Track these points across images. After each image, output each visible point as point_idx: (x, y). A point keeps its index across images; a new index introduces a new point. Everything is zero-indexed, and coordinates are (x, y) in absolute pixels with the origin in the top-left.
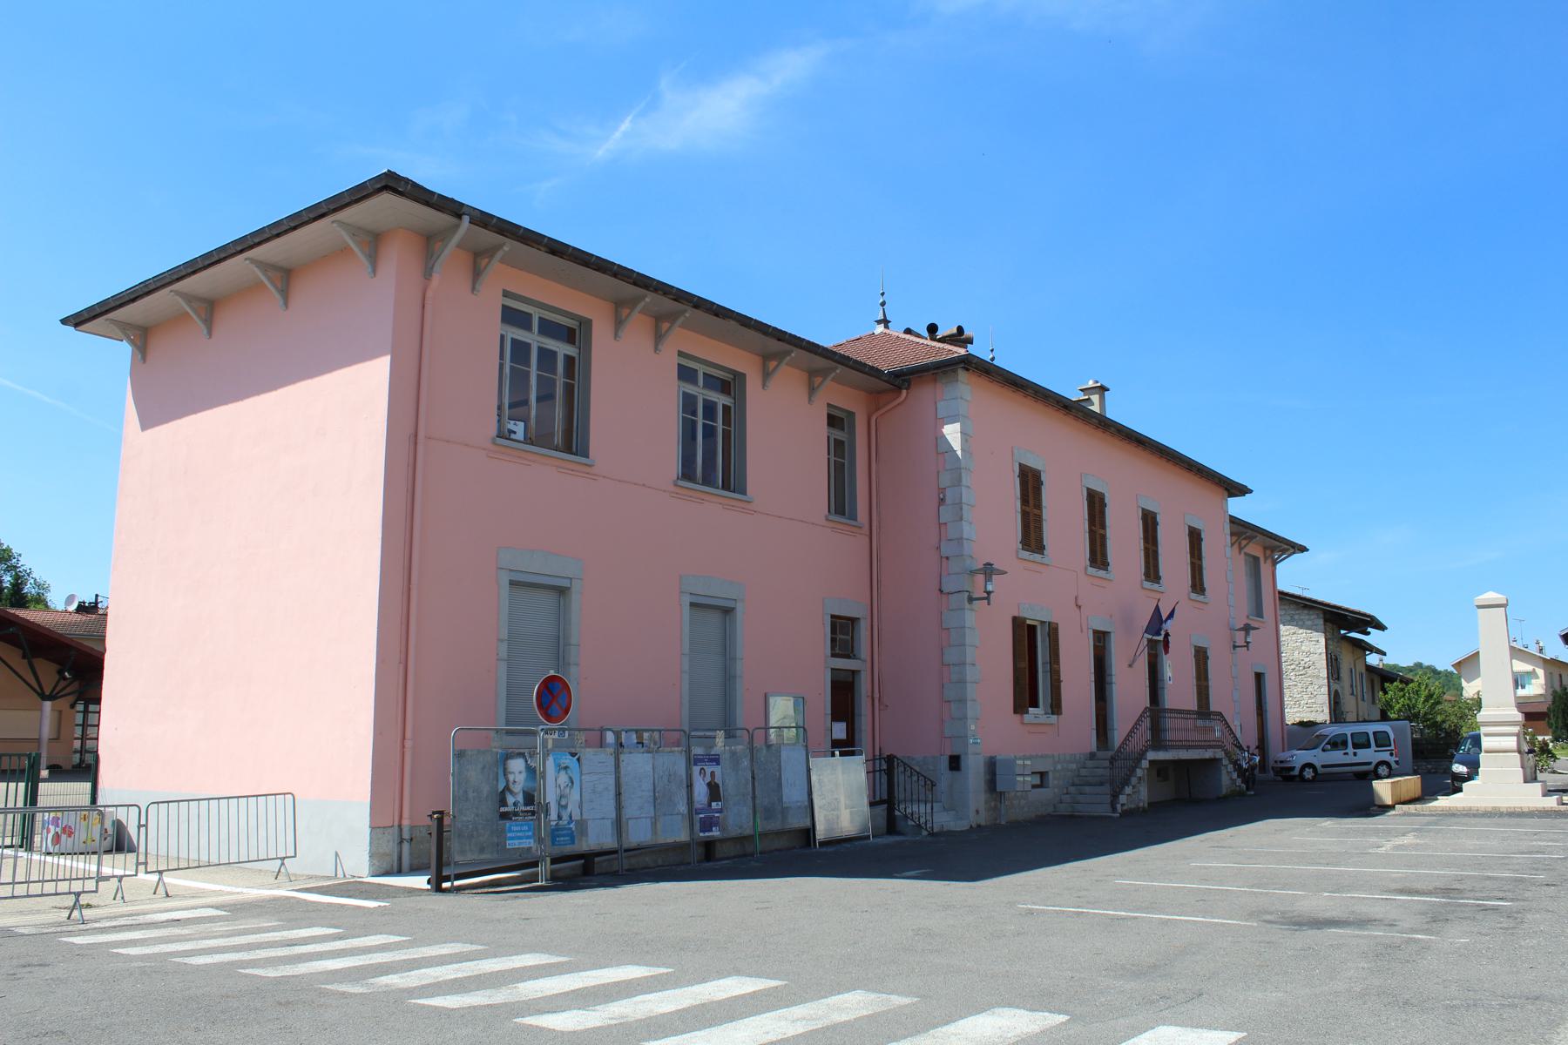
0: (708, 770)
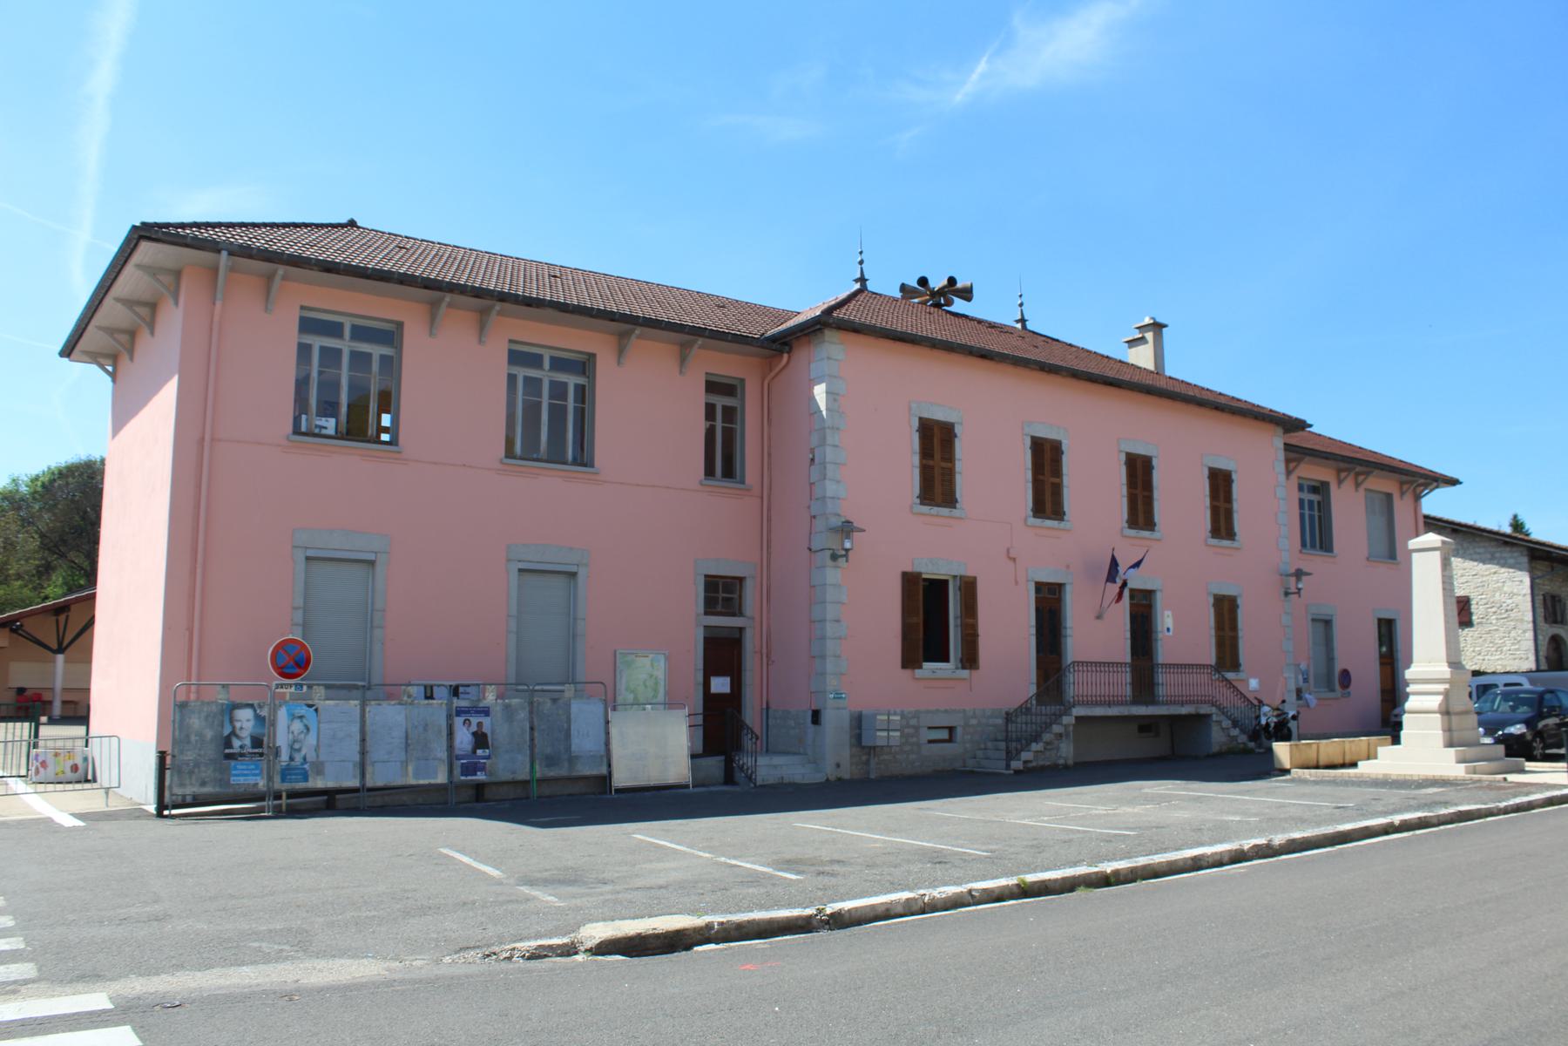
0: (474, 720)
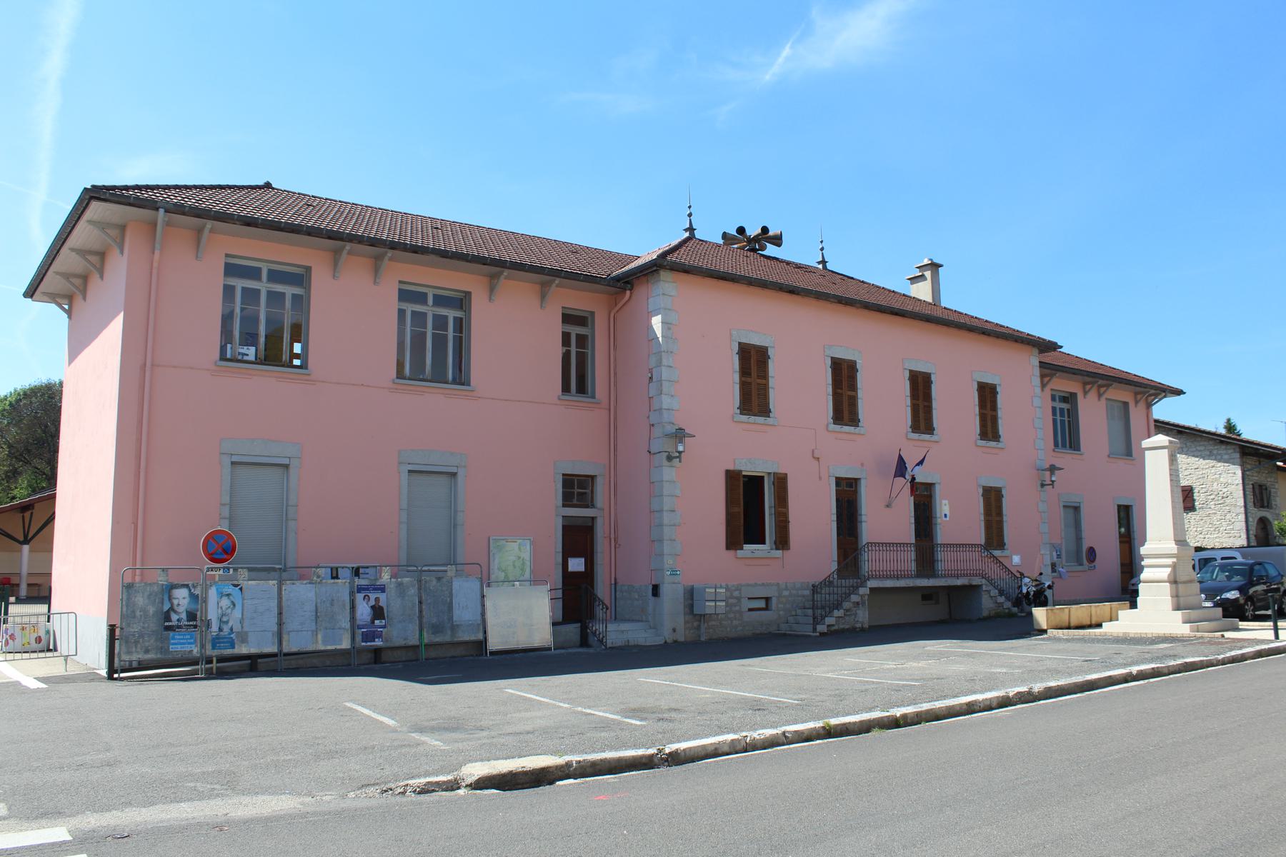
0: (373, 596)
